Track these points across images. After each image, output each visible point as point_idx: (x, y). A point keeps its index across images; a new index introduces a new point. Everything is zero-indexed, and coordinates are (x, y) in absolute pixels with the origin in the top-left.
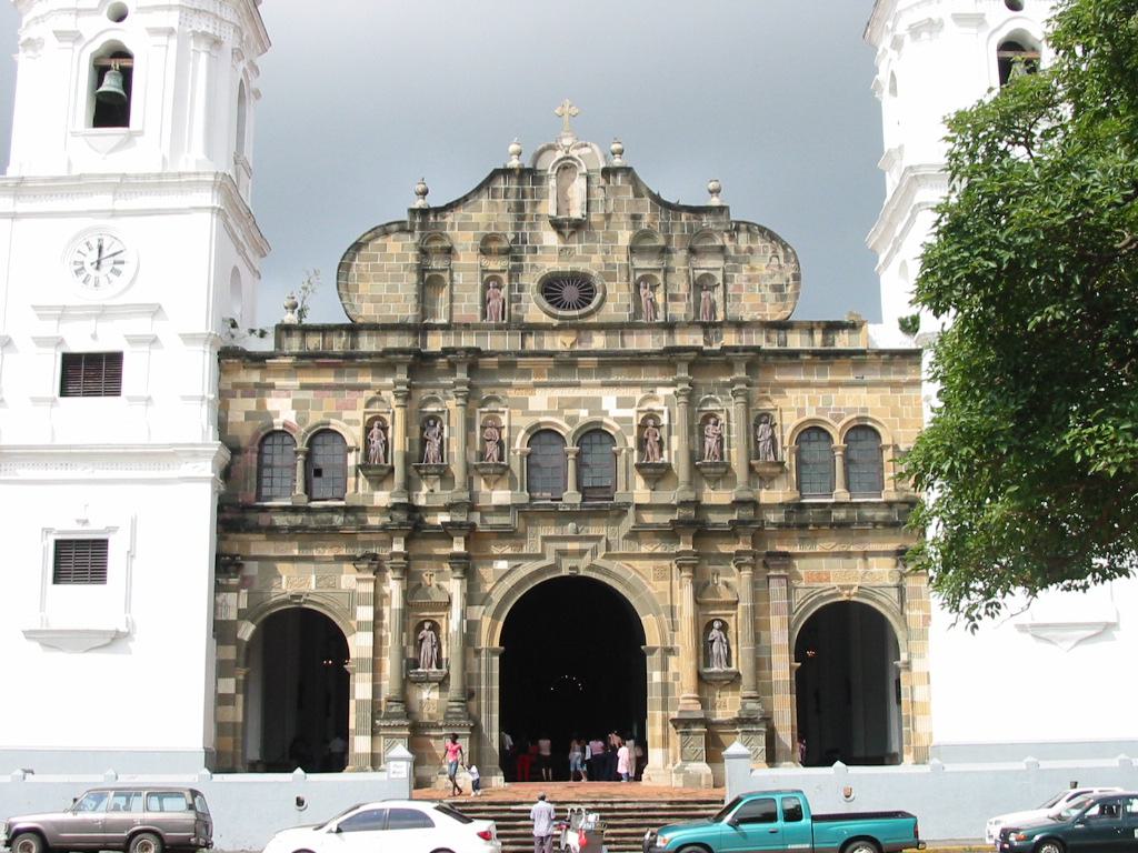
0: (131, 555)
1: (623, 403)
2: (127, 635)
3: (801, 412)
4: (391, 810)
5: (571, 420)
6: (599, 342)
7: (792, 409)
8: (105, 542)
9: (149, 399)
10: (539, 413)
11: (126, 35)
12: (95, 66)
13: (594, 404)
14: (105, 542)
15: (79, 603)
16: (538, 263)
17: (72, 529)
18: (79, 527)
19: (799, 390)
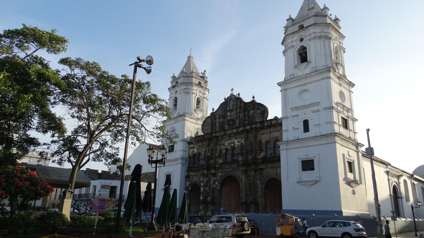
0: (319, 162)
1: (238, 142)
2: (319, 181)
3: (266, 139)
4: (136, 205)
5: (231, 146)
6: (235, 131)
7: (264, 139)
8: (313, 160)
9: (319, 124)
10: (226, 146)
11: (303, 44)
12: (299, 54)
13: (234, 143)
14: (313, 160)
15: (308, 175)
16: (227, 119)
17: (305, 158)
18: (306, 157)
19: (266, 134)
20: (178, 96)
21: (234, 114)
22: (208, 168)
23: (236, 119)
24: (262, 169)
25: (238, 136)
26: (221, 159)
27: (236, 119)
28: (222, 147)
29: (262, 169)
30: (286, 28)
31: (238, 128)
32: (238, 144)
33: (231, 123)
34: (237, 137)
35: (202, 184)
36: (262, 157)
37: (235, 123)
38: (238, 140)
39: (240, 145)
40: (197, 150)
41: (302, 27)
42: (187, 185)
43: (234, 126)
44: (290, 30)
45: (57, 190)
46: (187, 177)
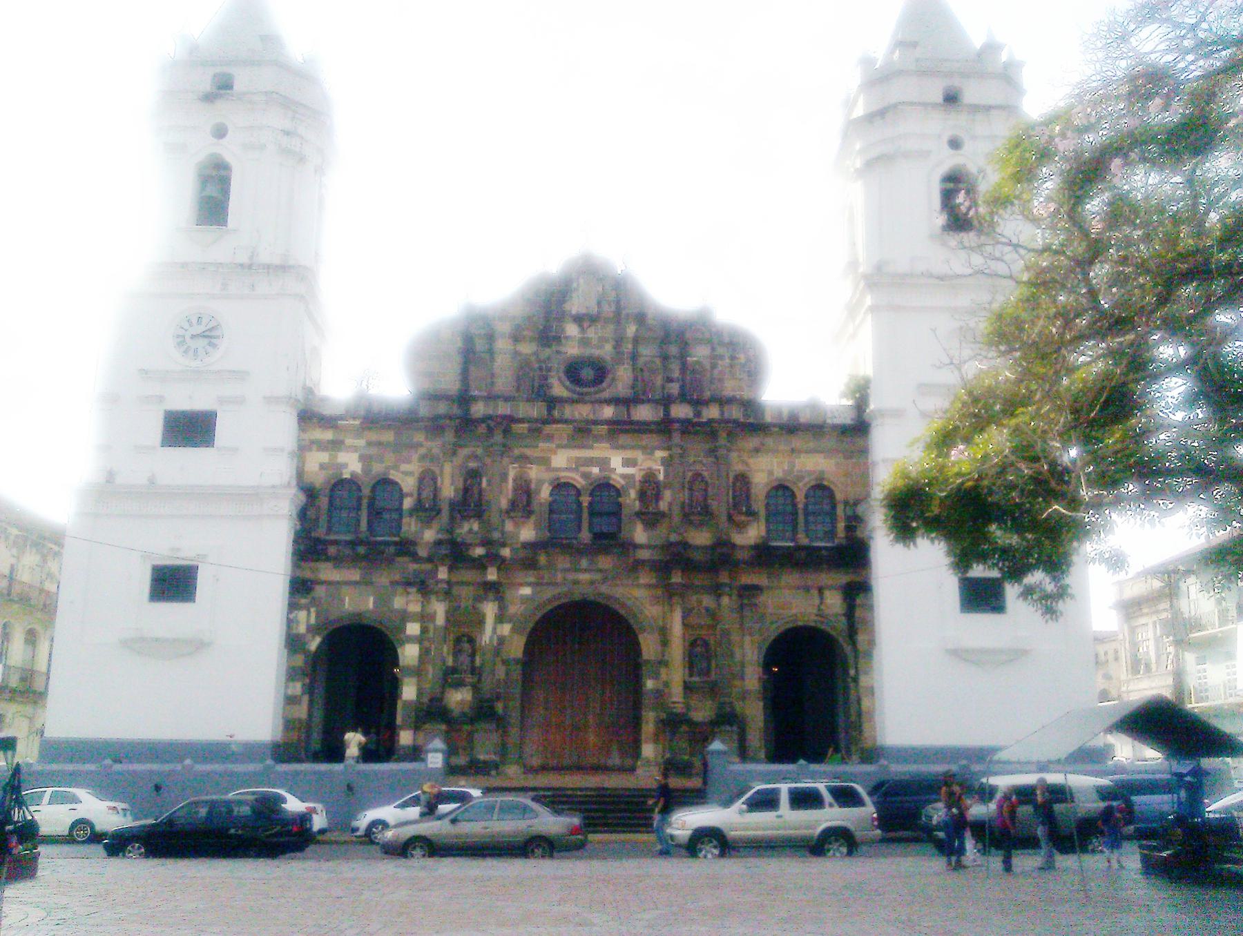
5: (586, 476)
7: (763, 471)
13: (604, 463)
15: (172, 614)
16: (563, 349)
20: (229, 151)
21: (603, 340)
22: (455, 553)
23: (618, 360)
24: (757, 589)
25: (623, 439)
26: (436, 525)
27: (618, 360)
28: (534, 472)
29: (757, 589)
30: (879, 79)
31: (625, 402)
32: (630, 471)
33: (587, 374)
34: (620, 442)
35: (413, 629)
36: (752, 542)
37: (613, 379)
38: (629, 454)
39: (638, 478)
40: (364, 459)
41: (951, 99)
42: (302, 629)
43: (604, 390)
44: (899, 91)
45: (431, 763)
46: (300, 588)
